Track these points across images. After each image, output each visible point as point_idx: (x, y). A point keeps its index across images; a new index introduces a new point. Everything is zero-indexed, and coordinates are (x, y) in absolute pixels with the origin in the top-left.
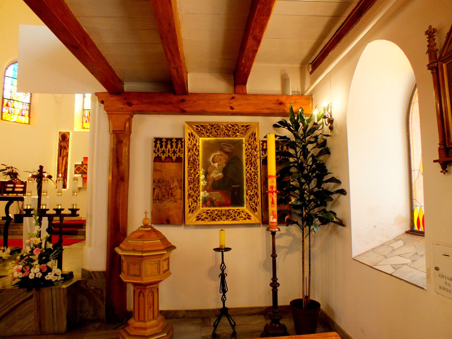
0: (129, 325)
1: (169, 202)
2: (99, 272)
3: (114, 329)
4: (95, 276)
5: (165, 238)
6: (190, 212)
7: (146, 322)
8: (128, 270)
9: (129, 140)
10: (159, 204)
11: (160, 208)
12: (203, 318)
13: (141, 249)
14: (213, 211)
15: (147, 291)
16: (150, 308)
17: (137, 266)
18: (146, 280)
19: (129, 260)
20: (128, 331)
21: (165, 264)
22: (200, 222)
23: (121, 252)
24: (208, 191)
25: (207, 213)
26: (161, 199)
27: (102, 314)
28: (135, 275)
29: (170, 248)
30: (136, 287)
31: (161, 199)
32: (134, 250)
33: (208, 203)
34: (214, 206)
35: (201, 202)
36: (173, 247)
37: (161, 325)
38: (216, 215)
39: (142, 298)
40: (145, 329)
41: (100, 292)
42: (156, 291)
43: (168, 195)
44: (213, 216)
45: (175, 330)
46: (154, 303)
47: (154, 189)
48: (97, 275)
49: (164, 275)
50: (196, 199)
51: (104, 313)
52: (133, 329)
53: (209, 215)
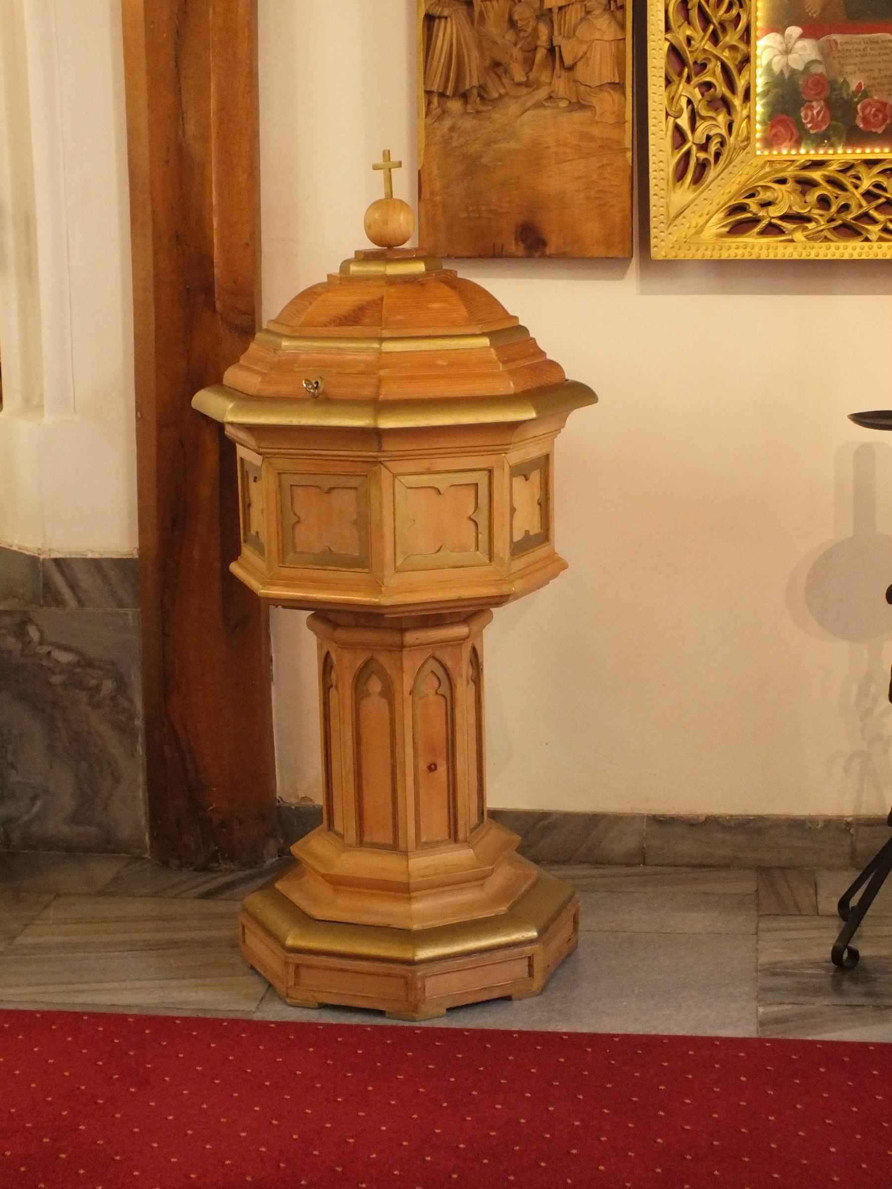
0: (301, 863)
1: (539, 105)
2: (96, 565)
3: (206, 896)
4: (73, 586)
5: (523, 330)
6: (680, 176)
7: (405, 853)
8: (287, 525)
9: (156, 266)
10: (468, 123)
11: (474, 148)
12: (762, 870)
13: (367, 392)
14: (847, 168)
15: (411, 662)
16: (432, 768)
17: (344, 501)
18: (401, 590)
19: (282, 464)
20: (296, 897)
21: (524, 493)
22: (755, 246)
23: (233, 411)
24: (811, 31)
25: (806, 185)
26: (482, 88)
27: (130, 809)
28: (331, 559)
29: (560, 394)
30: (342, 635)
31: (482, 88)
32: (322, 399)
33: (813, 112)
34: (855, 136)
35: (759, 108)
36: (582, 394)
37: (501, 877)
38: (868, 195)
39: (375, 705)
40: (403, 890)
41: (109, 686)
42: (466, 670)
43: (529, 62)
44: (846, 207)
45: (583, 923)
46: (456, 749)
47: (430, 19)
48: (86, 581)
49: (520, 563)
50: (721, 89)
51: (141, 810)
52: (324, 890)
53: (813, 196)
